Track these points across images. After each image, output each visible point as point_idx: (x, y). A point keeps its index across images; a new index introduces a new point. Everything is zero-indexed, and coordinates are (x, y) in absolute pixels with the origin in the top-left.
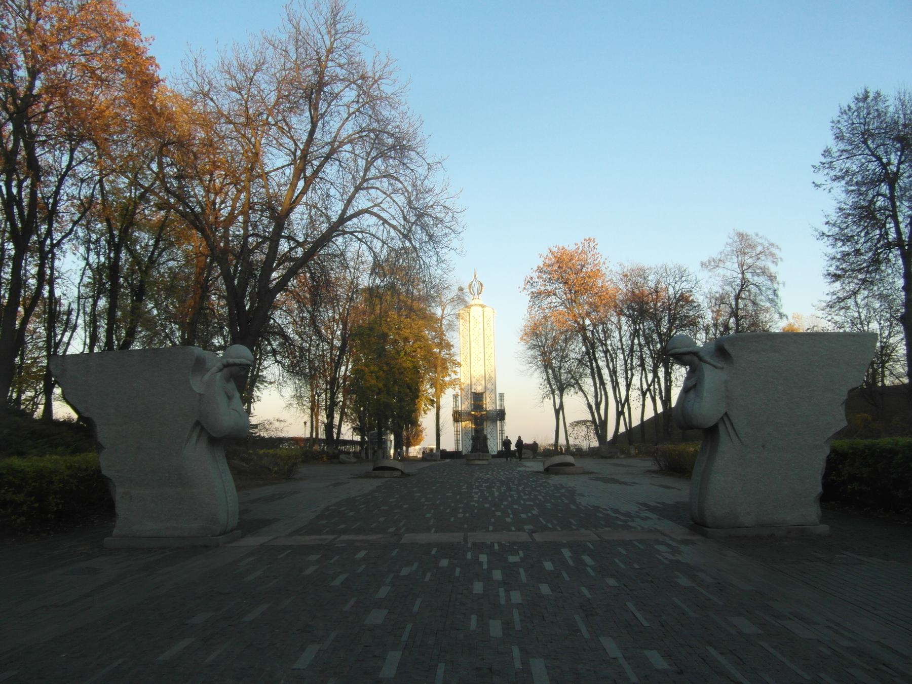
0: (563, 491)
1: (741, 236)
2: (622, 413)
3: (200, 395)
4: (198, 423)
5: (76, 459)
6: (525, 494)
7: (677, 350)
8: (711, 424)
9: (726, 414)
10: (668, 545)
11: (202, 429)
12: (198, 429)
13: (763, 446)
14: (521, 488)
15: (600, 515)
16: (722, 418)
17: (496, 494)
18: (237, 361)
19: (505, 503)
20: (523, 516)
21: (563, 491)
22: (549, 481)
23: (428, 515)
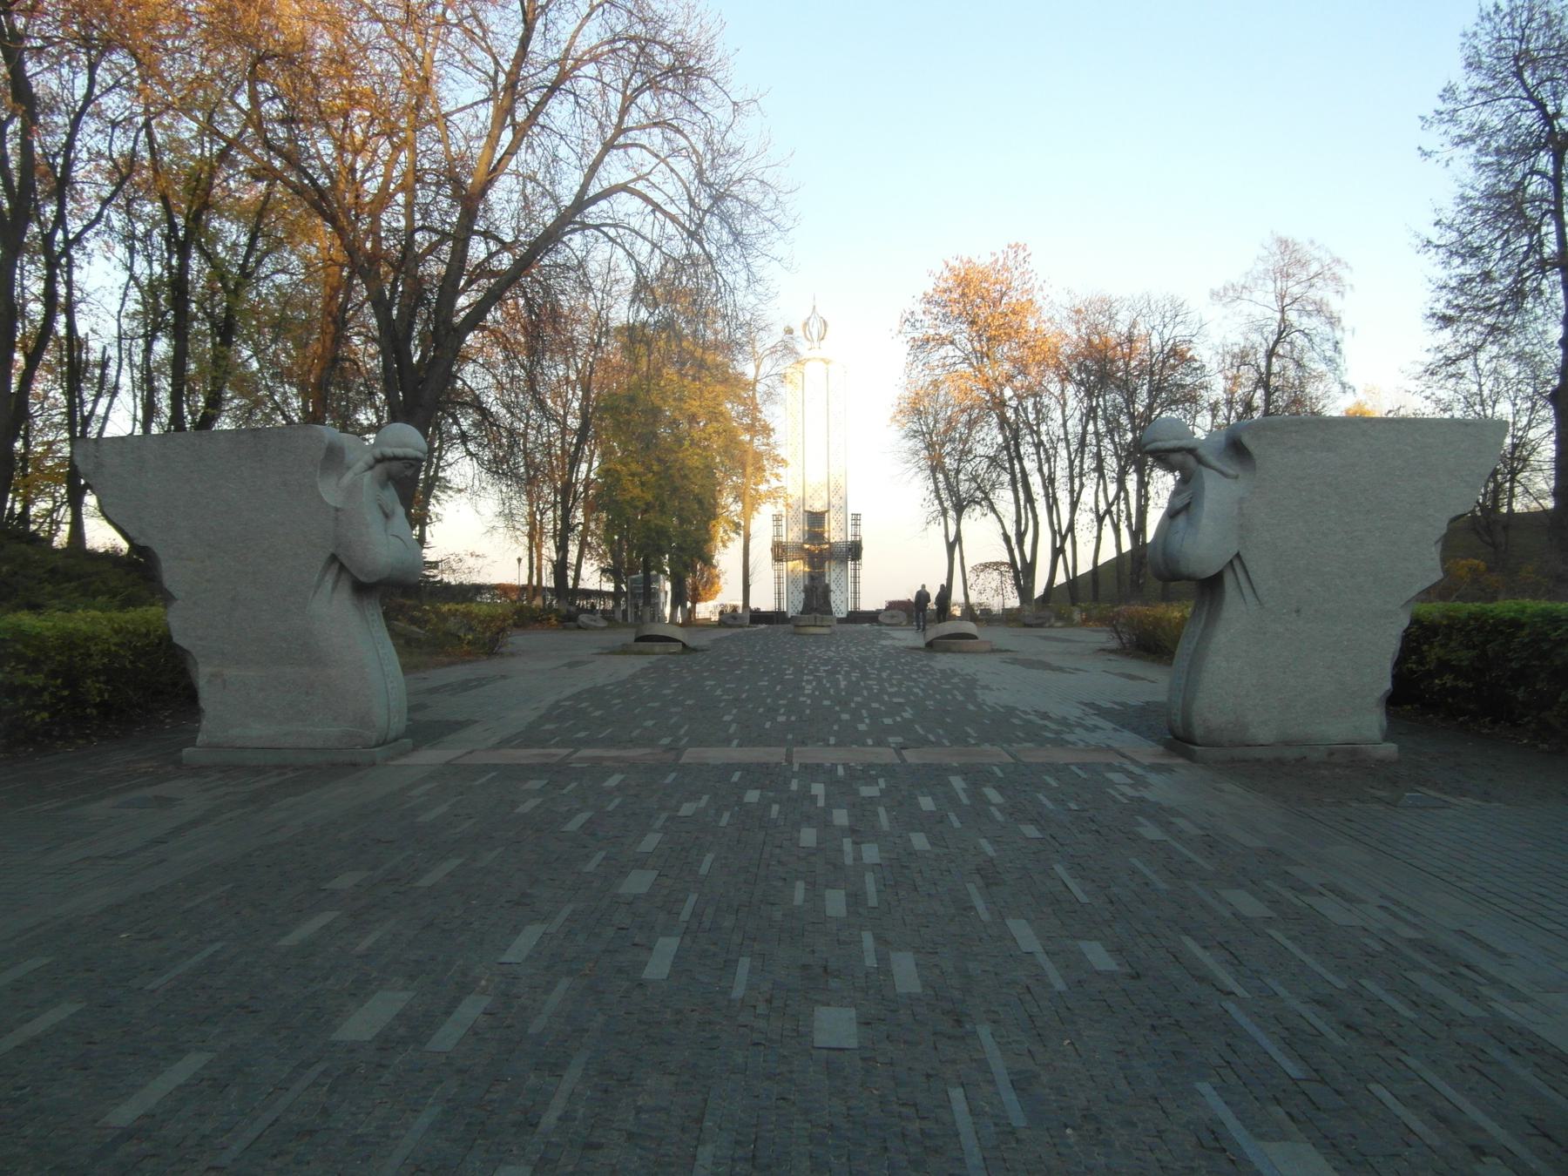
0: (956, 680)
1: (1284, 244)
4: (334, 558)
6: (892, 685)
8: (1211, 572)
9: (1238, 555)
11: (342, 568)
12: (336, 566)
14: (884, 675)
17: (843, 684)
18: (399, 452)
19: (859, 699)
21: (956, 680)
23: (727, 718)
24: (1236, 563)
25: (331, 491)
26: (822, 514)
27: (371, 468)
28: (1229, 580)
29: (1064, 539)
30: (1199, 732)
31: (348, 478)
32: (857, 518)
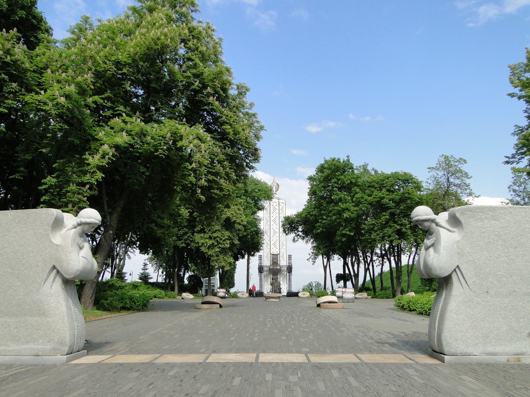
0: (330, 321)
1: (446, 158)
2: (368, 269)
3: (57, 245)
4: (54, 267)
5: (149, 292)
6: (304, 324)
7: (419, 218)
8: (446, 274)
9: (458, 267)
10: (414, 368)
11: (58, 272)
12: (55, 271)
13: (487, 292)
14: (301, 318)
15: (359, 341)
16: (455, 270)
17: (284, 322)
18: (88, 220)
19: (289, 330)
20: (302, 340)
21: (330, 321)
22: (320, 314)
23: (232, 339)
24: (457, 270)
25: (57, 239)
26: (277, 255)
27: (75, 228)
28: (454, 277)
29: (369, 265)
30: (446, 349)
31: (64, 230)
32: (290, 257)
